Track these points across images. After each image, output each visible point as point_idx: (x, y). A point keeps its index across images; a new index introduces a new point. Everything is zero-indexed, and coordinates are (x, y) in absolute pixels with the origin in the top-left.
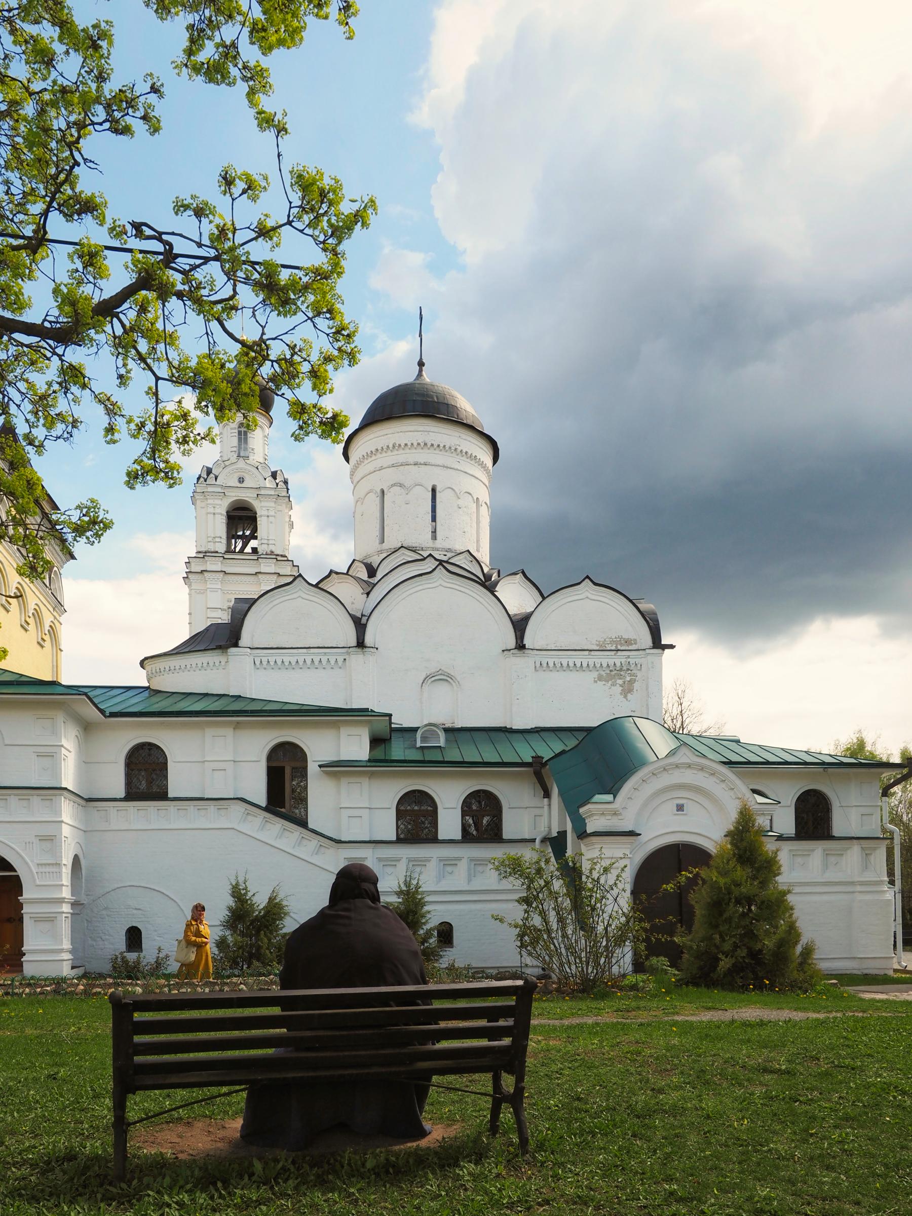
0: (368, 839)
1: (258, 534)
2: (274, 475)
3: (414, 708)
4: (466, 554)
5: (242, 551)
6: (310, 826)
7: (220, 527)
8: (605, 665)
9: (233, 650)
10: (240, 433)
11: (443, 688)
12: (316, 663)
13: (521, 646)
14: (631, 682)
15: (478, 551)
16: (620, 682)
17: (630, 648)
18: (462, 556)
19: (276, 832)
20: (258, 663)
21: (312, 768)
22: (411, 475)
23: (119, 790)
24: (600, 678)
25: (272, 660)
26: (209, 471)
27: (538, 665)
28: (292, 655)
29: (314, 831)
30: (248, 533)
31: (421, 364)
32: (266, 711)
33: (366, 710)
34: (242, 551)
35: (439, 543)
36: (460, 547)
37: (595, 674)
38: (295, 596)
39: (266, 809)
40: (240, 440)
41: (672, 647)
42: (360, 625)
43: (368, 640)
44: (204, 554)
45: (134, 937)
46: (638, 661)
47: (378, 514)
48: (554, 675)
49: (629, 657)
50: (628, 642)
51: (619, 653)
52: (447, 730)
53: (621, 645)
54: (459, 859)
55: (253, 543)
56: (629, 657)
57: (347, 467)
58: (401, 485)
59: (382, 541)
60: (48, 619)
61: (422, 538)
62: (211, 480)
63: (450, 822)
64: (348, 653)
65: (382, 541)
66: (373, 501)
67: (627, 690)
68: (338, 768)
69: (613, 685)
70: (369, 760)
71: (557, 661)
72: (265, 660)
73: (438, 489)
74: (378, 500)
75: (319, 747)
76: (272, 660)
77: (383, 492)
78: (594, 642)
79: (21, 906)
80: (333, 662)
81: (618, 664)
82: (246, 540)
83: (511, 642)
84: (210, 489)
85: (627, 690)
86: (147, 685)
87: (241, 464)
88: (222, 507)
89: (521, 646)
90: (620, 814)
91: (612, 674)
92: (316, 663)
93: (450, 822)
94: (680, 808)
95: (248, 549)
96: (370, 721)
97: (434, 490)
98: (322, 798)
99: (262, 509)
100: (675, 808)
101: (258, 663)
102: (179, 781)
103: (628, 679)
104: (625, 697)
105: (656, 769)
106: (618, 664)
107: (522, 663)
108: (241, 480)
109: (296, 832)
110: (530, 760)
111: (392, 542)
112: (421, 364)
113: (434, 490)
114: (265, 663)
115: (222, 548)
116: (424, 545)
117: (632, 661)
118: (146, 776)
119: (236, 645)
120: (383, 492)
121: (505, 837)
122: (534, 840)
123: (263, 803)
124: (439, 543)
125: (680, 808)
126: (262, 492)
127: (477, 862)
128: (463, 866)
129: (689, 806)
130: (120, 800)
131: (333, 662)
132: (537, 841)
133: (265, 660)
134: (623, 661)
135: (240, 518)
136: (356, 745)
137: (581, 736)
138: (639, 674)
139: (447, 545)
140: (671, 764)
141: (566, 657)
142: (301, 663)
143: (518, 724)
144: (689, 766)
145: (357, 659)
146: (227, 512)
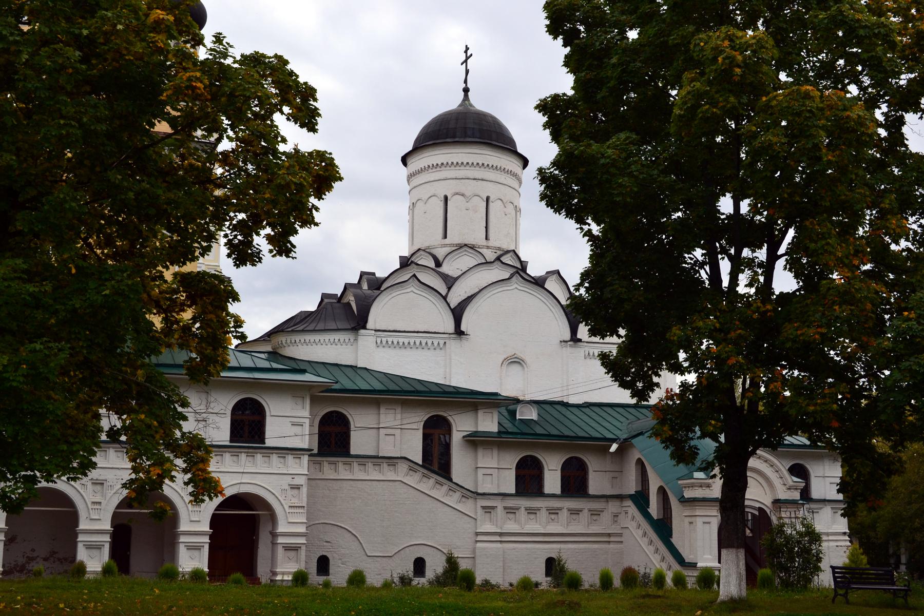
4: (511, 254)
9: (362, 331)
11: (516, 367)
12: (424, 344)
18: (509, 255)
19: (428, 484)
20: (379, 342)
21: (457, 437)
22: (469, 188)
25: (390, 340)
28: (409, 337)
31: (466, 90)
35: (493, 242)
38: (408, 290)
42: (458, 313)
54: (560, 509)
58: (463, 195)
59: (445, 237)
61: (477, 237)
63: (552, 481)
68: (475, 441)
72: (384, 340)
73: (491, 199)
74: (442, 204)
76: (390, 340)
77: (446, 198)
80: (436, 344)
83: (567, 335)
92: (424, 344)
93: (552, 481)
98: (461, 462)
101: (379, 342)
102: (359, 442)
111: (454, 237)
112: (466, 90)
114: (384, 342)
119: (364, 328)
120: (446, 198)
127: (575, 512)
128: (564, 514)
131: (436, 344)
133: (384, 340)
142: (412, 344)
143: (827, 498)
145: (454, 345)
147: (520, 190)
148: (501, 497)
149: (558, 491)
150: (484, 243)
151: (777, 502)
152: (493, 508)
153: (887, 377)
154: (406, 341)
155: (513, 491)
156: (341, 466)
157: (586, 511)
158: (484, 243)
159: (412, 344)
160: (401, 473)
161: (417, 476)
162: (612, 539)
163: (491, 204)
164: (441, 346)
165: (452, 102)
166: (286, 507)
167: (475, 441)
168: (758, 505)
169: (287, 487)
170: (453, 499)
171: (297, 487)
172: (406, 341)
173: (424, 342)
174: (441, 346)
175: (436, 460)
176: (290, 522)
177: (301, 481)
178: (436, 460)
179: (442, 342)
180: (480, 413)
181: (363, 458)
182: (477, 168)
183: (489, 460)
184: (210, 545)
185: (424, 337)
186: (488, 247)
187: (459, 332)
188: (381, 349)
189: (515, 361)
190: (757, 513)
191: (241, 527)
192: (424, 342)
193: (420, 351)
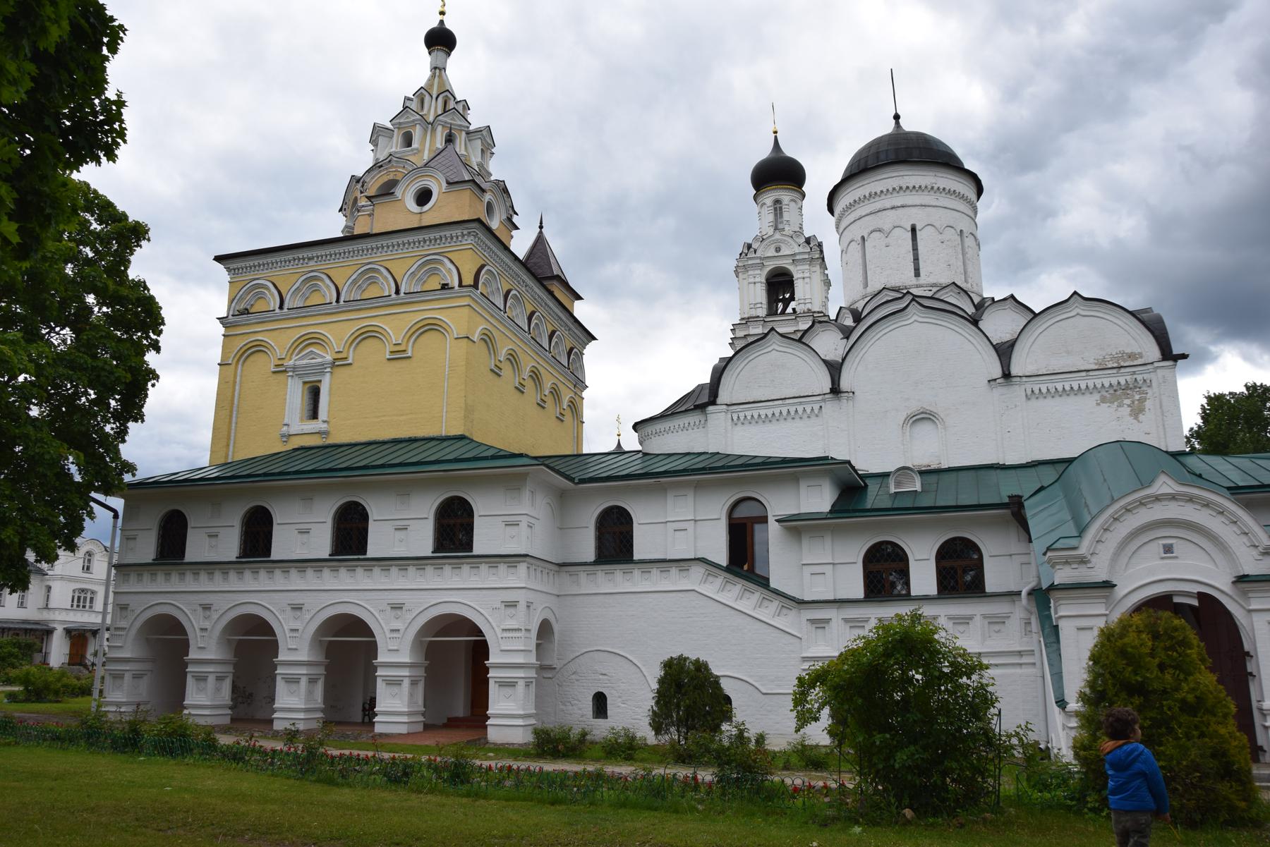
0: (832, 598)
1: (796, 296)
2: (808, 241)
3: (876, 449)
4: (953, 287)
5: (783, 312)
6: (773, 584)
7: (759, 294)
8: (1107, 385)
10: (775, 209)
11: (925, 429)
12: (792, 413)
13: (1007, 375)
14: (1142, 400)
15: (966, 281)
16: (1128, 402)
17: (1135, 363)
19: (734, 594)
23: (590, 555)
24: (1103, 400)
25: (749, 414)
26: (749, 246)
27: (1029, 392)
28: (769, 407)
29: (777, 593)
30: (787, 296)
32: (289, 473)
33: (826, 458)
34: (783, 312)
36: (945, 281)
37: (1097, 396)
39: (727, 569)
40: (776, 215)
41: (1184, 356)
43: (845, 384)
44: (746, 321)
45: (600, 704)
46: (1146, 376)
47: (860, 261)
48: (1049, 401)
49: (1134, 373)
50: (1131, 356)
51: (1123, 370)
52: (921, 473)
53: (1124, 361)
54: (971, 618)
55: (793, 305)
56: (1134, 373)
57: (832, 220)
59: (866, 285)
60: (566, 397)
61: (905, 277)
62: (751, 255)
64: (824, 400)
65: (866, 285)
66: (855, 248)
67: (1137, 411)
68: (798, 526)
69: (1119, 406)
70: (831, 512)
71: (1051, 386)
72: (742, 415)
75: (780, 503)
78: (1092, 361)
79: (487, 670)
80: (808, 411)
81: (1123, 382)
82: (786, 303)
83: (997, 371)
84: (750, 262)
85: (1137, 411)
86: (640, 448)
87: (778, 236)
88: (761, 276)
89: (1007, 375)
90: (1089, 561)
91: (1116, 394)
94: (1168, 549)
95: (789, 310)
96: (831, 470)
97: (914, 230)
98: (782, 560)
99: (797, 272)
100: (1162, 550)
102: (645, 544)
103: (1137, 397)
104: (1136, 418)
105: (1129, 504)
106: (1123, 382)
107: (1017, 392)
108: (778, 249)
109: (758, 594)
110: (1007, 500)
111: (875, 286)
112: (897, 117)
113: (914, 230)
115: (762, 312)
116: (908, 283)
117: (1139, 378)
118: (615, 542)
120: (863, 238)
121: (988, 590)
122: (1019, 593)
123: (724, 563)
124: (923, 279)
125: (1168, 549)
126: (969, 242)
129: (1179, 546)
130: (419, 561)
131: (808, 411)
132: (1024, 593)
133: (742, 415)
134: (1128, 378)
135: (780, 283)
136: (818, 498)
137: (1061, 468)
138: (1149, 391)
139: (932, 280)
140: (1148, 496)
141: (1058, 383)
143: (668, 558)
144: (1173, 497)
145: (830, 407)
146: (767, 280)
147: (978, 204)
148: (1008, 598)
149: (933, 590)
150: (914, 281)
151: (1242, 580)
152: (828, 621)
153: (58, 117)
154: (769, 413)
155: (859, 593)
156: (263, 574)
157: (978, 618)
158: (914, 281)
159: (777, 414)
160: (694, 579)
161: (719, 581)
162: (1025, 660)
163: (918, 233)
164: (816, 411)
165: (888, 128)
166: (498, 631)
167: (798, 526)
168: (1196, 589)
169: (499, 605)
170: (769, 611)
171: (512, 605)
172: (769, 413)
173: (792, 410)
174: (816, 411)
175: (743, 558)
176: (508, 649)
177: (521, 597)
178: (743, 558)
179: (816, 407)
180: (803, 486)
181: (385, 562)
182: (895, 194)
183: (819, 551)
184: (326, 677)
185: (792, 406)
186: (921, 286)
187: (835, 390)
188: (739, 427)
189: (923, 417)
190: (1195, 603)
191: (457, 656)
192: (792, 410)
193: (790, 423)
